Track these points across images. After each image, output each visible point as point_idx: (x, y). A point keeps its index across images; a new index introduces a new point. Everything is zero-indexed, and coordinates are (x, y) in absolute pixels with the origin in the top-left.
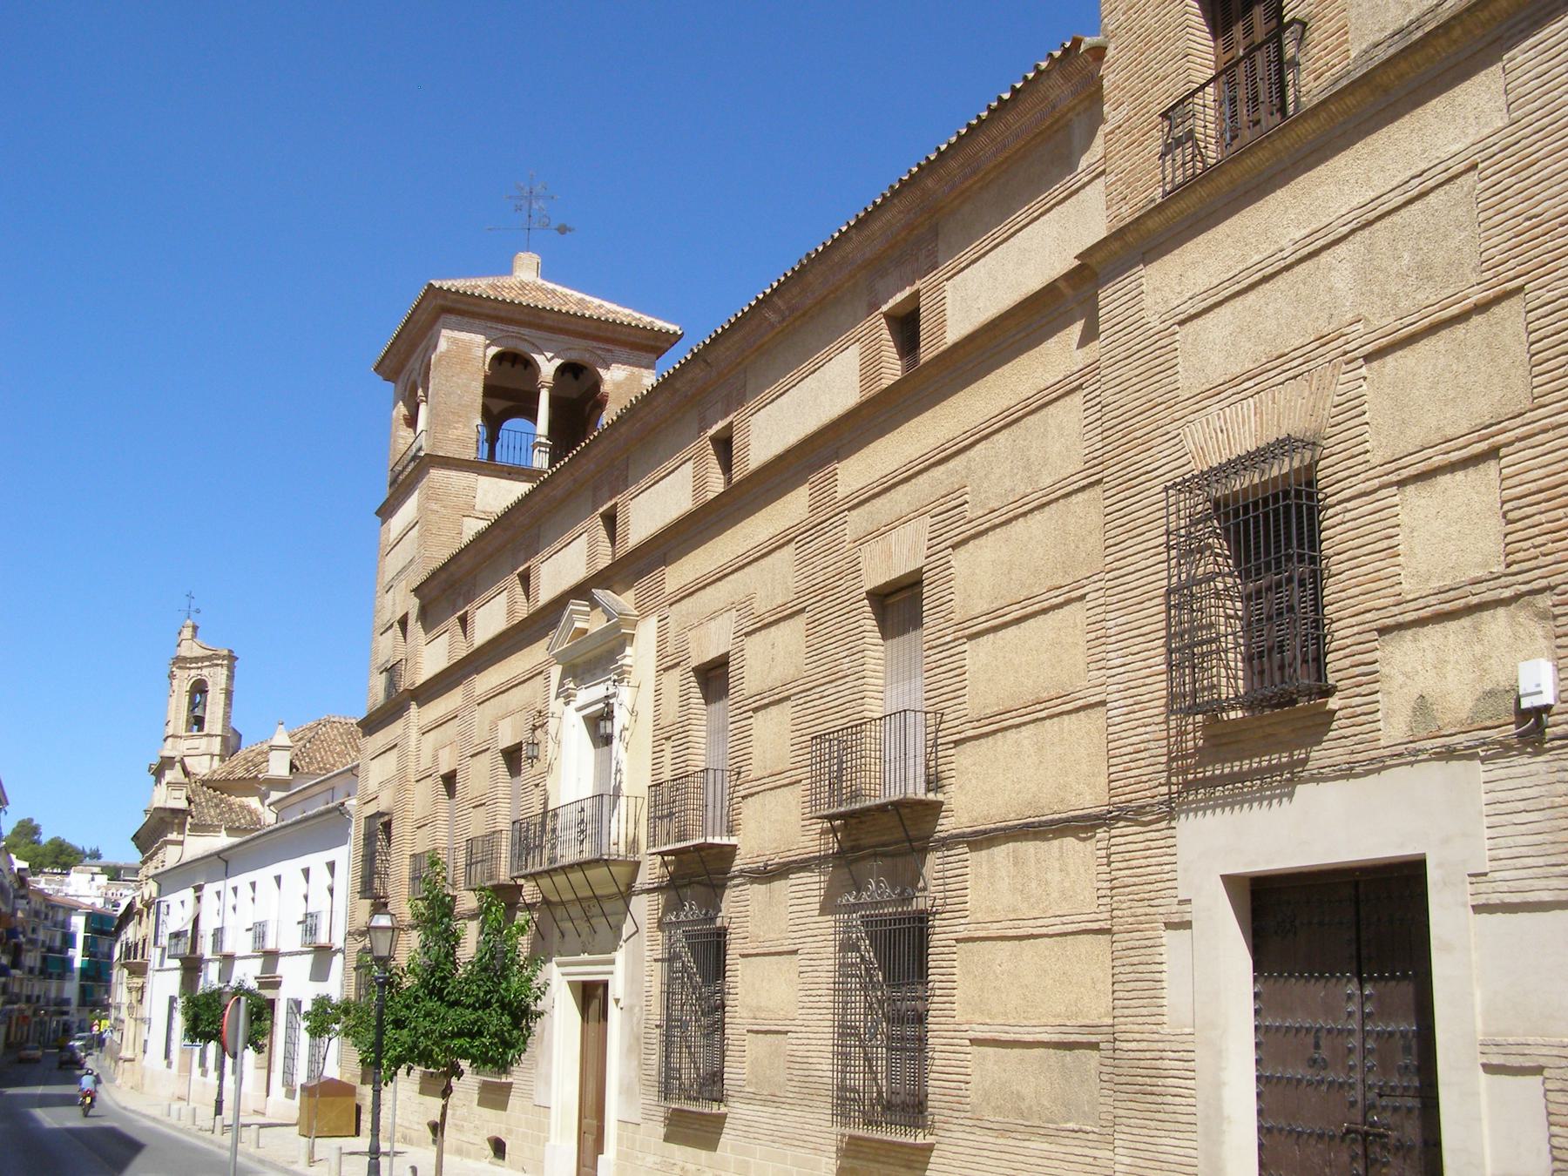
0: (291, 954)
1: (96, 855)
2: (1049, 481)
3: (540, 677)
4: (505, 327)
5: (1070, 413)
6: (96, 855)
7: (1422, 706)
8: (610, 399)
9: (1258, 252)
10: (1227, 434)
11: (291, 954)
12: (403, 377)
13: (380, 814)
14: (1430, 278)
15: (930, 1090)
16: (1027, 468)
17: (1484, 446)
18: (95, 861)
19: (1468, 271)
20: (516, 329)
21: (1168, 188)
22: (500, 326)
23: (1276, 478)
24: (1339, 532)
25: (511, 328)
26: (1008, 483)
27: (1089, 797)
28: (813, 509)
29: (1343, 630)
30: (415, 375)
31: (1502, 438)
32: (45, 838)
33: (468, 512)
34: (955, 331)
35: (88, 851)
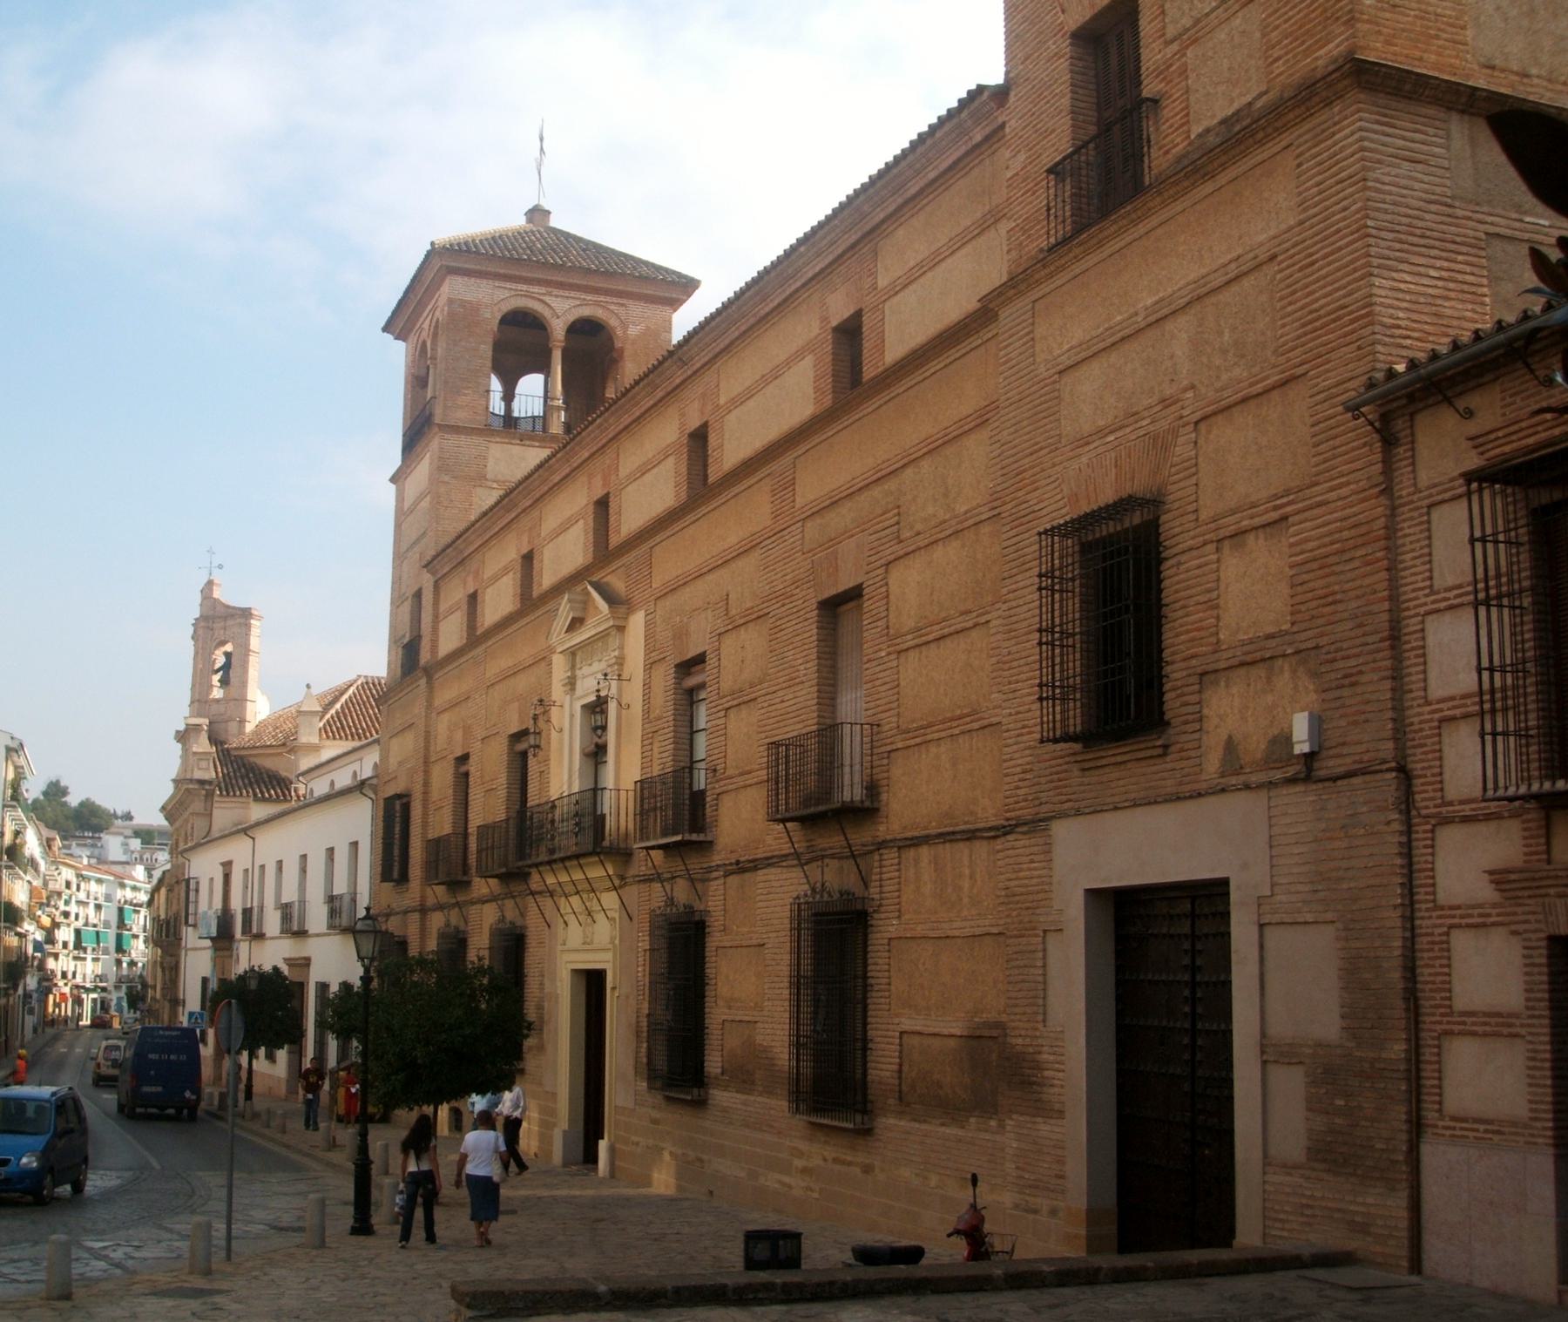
0: (318, 935)
1: (128, 817)
2: (963, 509)
3: (543, 664)
4: (513, 286)
5: (977, 448)
6: (128, 817)
7: (1230, 746)
8: (626, 354)
9: (1120, 313)
10: (1083, 482)
11: (318, 935)
12: (413, 338)
13: (399, 796)
14: (1243, 356)
15: (1546, 1013)
16: (946, 495)
17: (1275, 515)
18: (128, 823)
19: (1269, 353)
20: (525, 287)
21: (1052, 240)
22: (508, 285)
23: (1138, 526)
24: (1180, 579)
25: (520, 286)
26: (930, 510)
27: (989, 812)
28: (776, 516)
29: (1176, 673)
30: (424, 334)
31: (1288, 509)
32: (73, 800)
33: (481, 479)
34: (894, 352)
35: (119, 813)
